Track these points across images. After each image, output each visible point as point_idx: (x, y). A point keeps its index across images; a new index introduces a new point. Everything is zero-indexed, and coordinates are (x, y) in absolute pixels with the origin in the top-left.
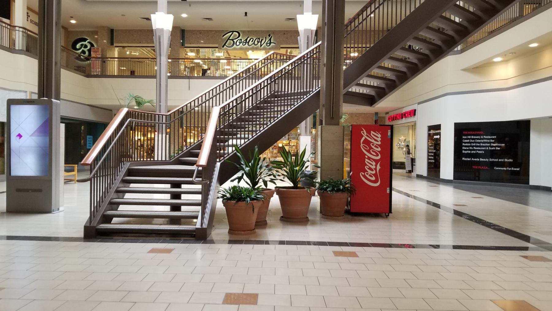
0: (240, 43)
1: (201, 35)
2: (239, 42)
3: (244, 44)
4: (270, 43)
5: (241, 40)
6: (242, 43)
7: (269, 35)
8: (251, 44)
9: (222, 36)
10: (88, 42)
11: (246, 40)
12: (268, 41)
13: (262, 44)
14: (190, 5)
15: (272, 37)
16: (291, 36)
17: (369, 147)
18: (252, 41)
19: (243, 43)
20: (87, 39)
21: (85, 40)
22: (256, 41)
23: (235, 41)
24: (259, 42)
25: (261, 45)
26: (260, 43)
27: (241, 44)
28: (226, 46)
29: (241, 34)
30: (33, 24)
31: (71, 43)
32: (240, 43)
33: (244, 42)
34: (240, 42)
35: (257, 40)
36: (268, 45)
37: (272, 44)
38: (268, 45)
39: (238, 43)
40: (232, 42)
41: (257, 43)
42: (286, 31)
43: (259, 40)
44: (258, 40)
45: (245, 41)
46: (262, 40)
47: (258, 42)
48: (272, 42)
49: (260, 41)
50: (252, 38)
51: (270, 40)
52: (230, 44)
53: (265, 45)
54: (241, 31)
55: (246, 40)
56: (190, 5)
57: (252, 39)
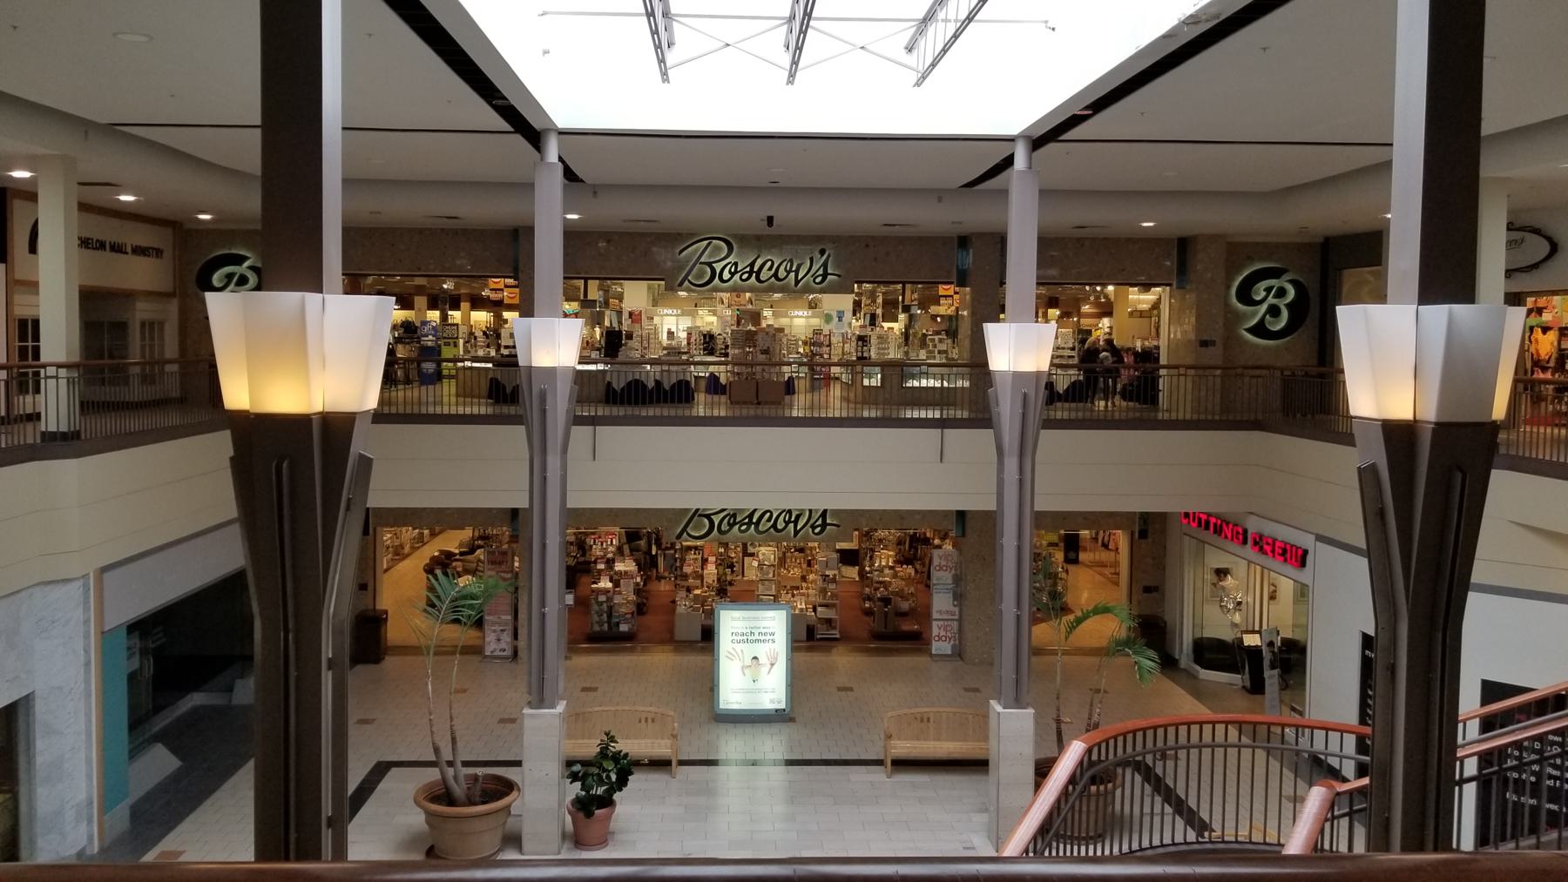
0: (732, 274)
1: (612, 248)
2: (729, 523)
3: (744, 528)
4: (825, 276)
5: (736, 264)
6: (737, 526)
7: (822, 252)
8: (765, 528)
9: (678, 251)
10: (251, 268)
11: (752, 265)
12: (820, 268)
13: (800, 278)
14: (595, 193)
15: (829, 256)
16: (888, 254)
17: (1247, 342)
18: (770, 269)
19: (741, 526)
20: (245, 258)
21: (239, 260)
22: (782, 268)
23: (718, 267)
24: (789, 521)
25: (797, 282)
26: (792, 275)
27: (737, 277)
28: (690, 282)
29: (735, 246)
30: (100, 251)
31: (193, 277)
32: (732, 274)
33: (746, 272)
34: (733, 270)
35: (785, 264)
36: (817, 530)
37: (829, 277)
38: (819, 280)
39: (726, 275)
40: (709, 270)
41: (784, 525)
42: (873, 238)
43: (790, 517)
44: (789, 264)
45: (748, 269)
46: (799, 266)
47: (787, 523)
48: (828, 521)
49: (793, 519)
50: (771, 260)
51: (825, 265)
52: (700, 275)
53: (808, 280)
54: (735, 236)
55: (752, 265)
56: (595, 193)
57: (769, 263)
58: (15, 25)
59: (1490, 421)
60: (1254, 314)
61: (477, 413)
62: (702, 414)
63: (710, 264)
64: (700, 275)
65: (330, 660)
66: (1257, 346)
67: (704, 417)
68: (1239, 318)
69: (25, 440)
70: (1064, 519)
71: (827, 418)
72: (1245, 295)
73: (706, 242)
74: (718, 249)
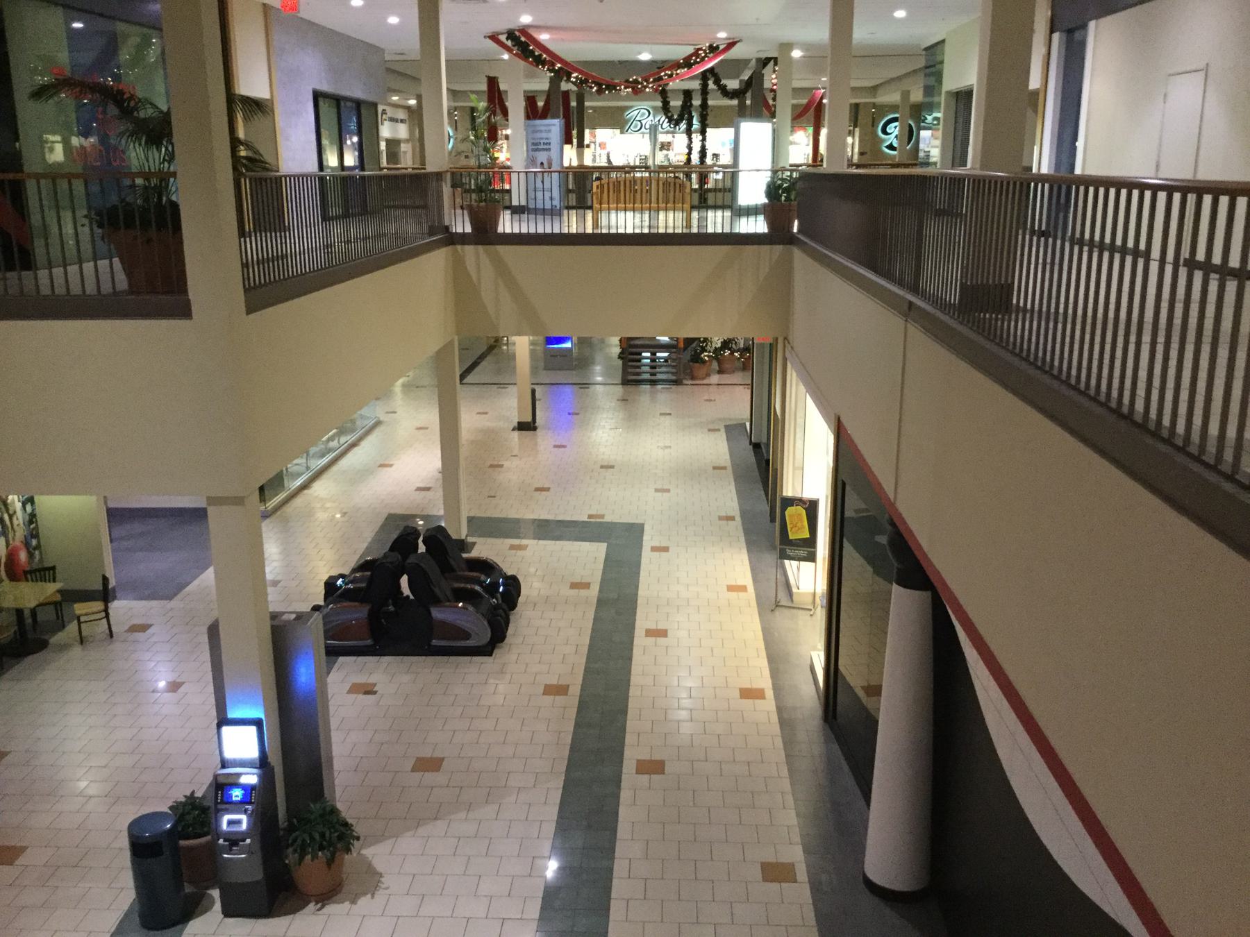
11: (659, 121)
17: (886, 153)
23: (644, 122)
52: (636, 126)
58: (864, 156)
59: (680, 109)
60: (889, 139)
61: (543, 232)
62: (508, 231)
63: (640, 121)
64: (636, 126)
65: (1185, 259)
66: (889, 154)
67: (512, 235)
68: (883, 141)
69: (111, 264)
70: (252, 853)
71: (561, 235)
72: (884, 132)
73: (637, 111)
74: (643, 114)
